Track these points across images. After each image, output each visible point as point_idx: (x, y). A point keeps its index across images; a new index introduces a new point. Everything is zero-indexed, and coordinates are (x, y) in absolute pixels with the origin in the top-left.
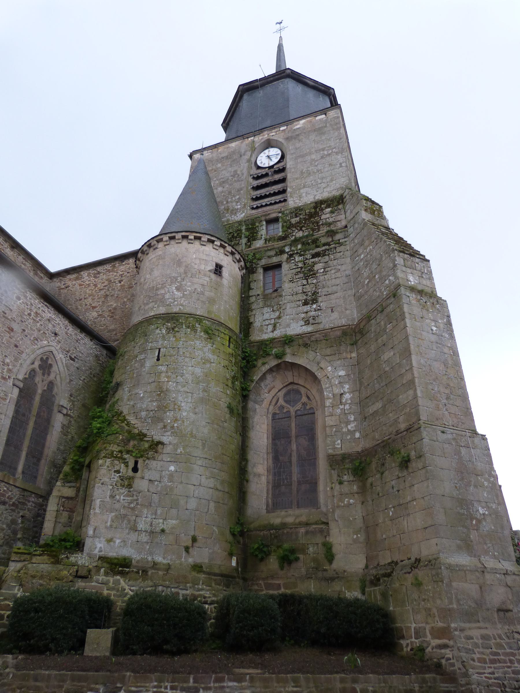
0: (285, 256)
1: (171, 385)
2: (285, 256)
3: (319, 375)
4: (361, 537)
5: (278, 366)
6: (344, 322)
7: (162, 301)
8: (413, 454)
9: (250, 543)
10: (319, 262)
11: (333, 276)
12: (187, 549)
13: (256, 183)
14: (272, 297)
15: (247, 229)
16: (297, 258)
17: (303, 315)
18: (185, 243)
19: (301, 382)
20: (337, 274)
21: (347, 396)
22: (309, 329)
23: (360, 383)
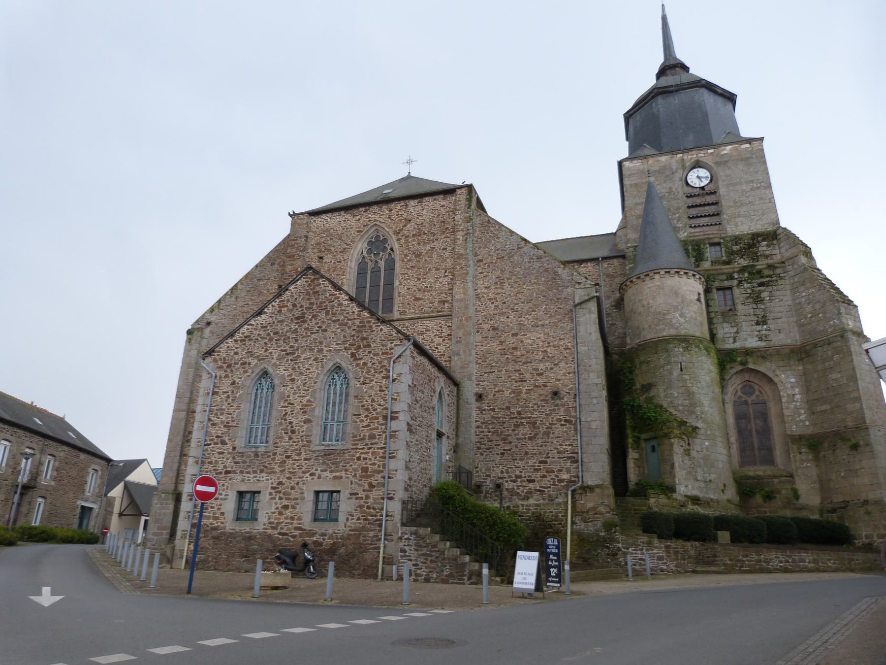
0: (735, 282)
1: (695, 389)
2: (735, 282)
3: (776, 380)
4: (817, 485)
5: (742, 371)
6: (789, 341)
7: (671, 325)
8: (861, 443)
9: (746, 489)
10: (765, 291)
11: (778, 304)
12: (723, 491)
13: (691, 202)
14: (730, 314)
15: (694, 250)
16: (746, 285)
17: (757, 333)
18: (676, 276)
19: (756, 381)
20: (781, 301)
21: (798, 396)
22: (763, 344)
23: (807, 388)
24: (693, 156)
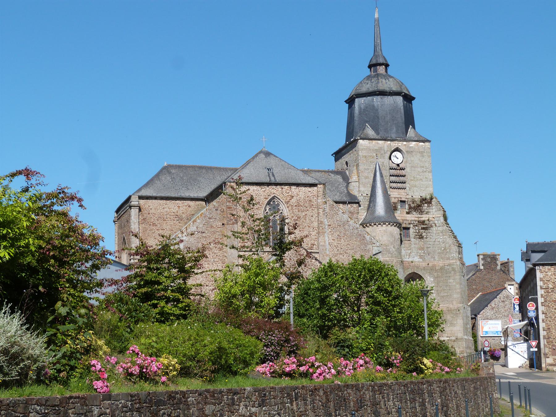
24: (395, 144)
